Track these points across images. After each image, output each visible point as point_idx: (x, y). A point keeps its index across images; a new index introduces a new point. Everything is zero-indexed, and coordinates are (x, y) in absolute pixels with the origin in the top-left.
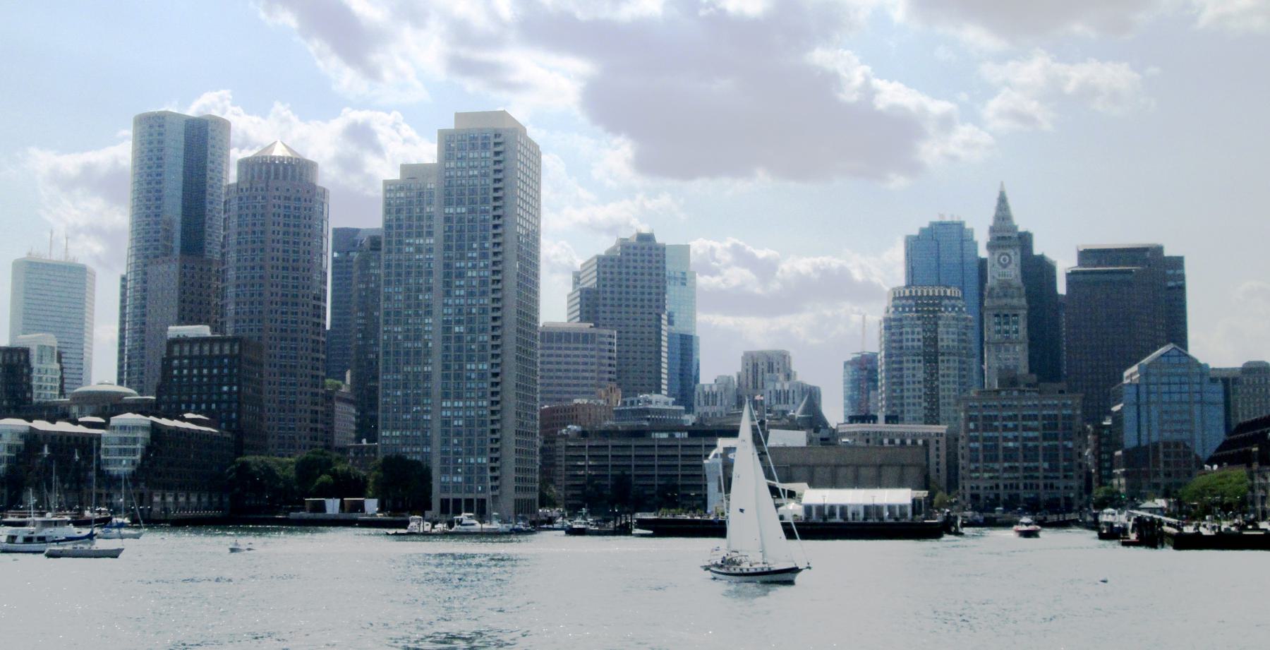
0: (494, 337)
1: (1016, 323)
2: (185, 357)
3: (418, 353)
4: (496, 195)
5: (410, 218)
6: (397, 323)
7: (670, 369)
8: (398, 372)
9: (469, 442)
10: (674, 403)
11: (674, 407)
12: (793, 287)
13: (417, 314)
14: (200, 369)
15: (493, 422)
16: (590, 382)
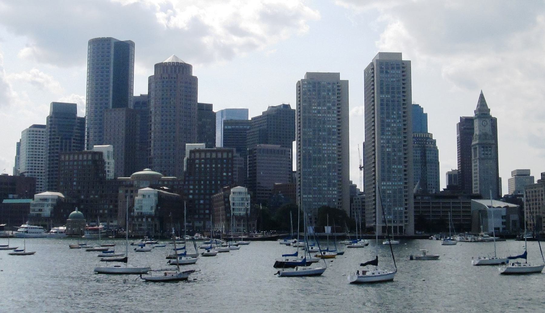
1: (490, 151)
6: (310, 145)
8: (310, 168)
13: (319, 142)
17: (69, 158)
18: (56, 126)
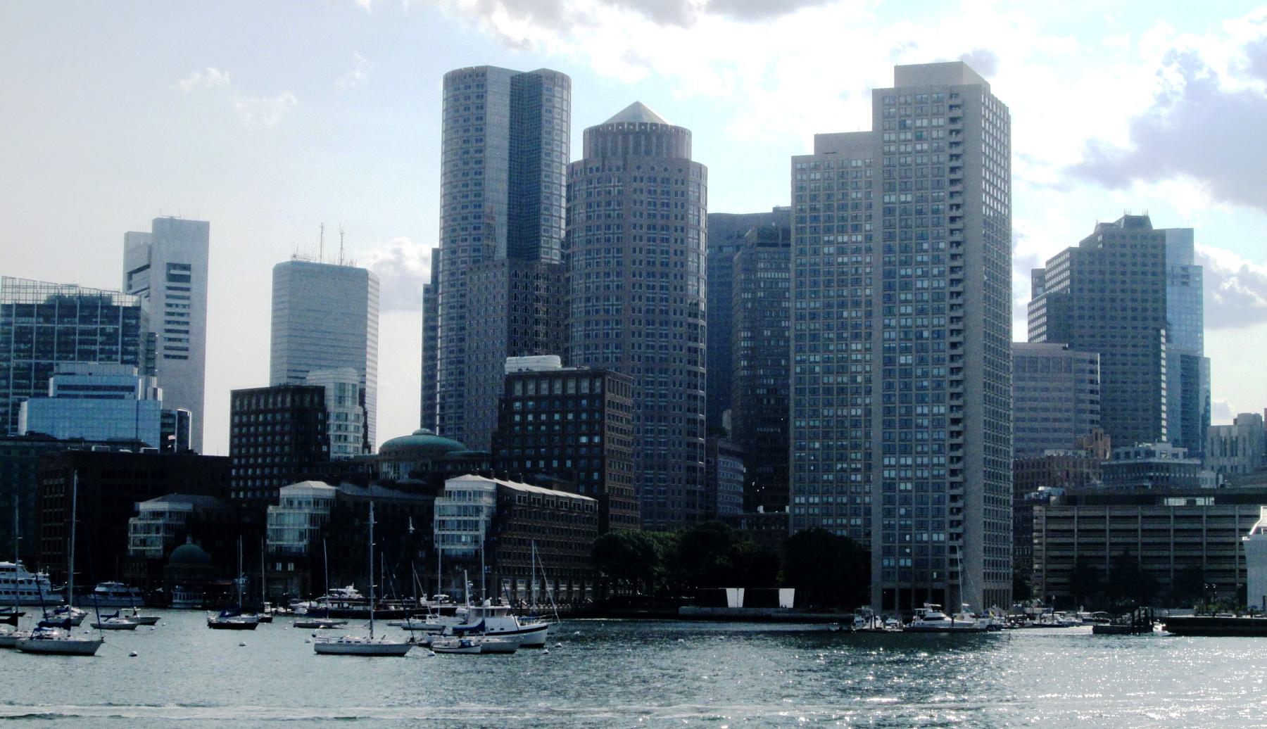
0: (952, 371)
2: (531, 398)
3: (842, 391)
4: (954, 176)
5: (829, 208)
6: (814, 350)
7: (1169, 404)
8: (815, 414)
9: (922, 512)
10: (1185, 456)
11: (1187, 461)
13: (840, 338)
14: (564, 414)
15: (953, 485)
16: (1065, 425)
17: (538, 389)
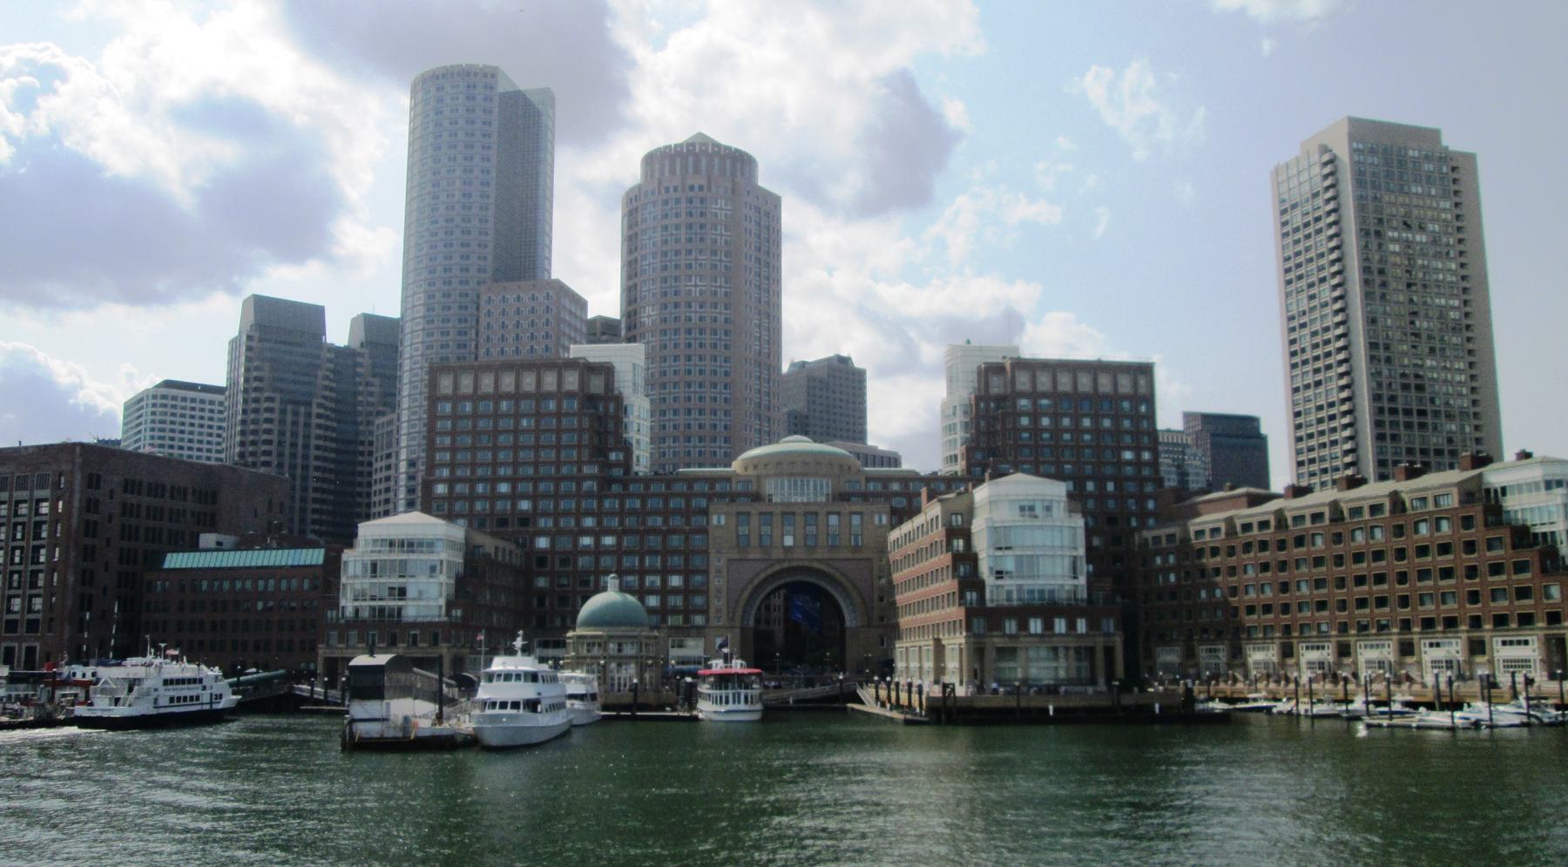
12: (1422, 709)
14: (1096, 418)
18: (267, 366)
